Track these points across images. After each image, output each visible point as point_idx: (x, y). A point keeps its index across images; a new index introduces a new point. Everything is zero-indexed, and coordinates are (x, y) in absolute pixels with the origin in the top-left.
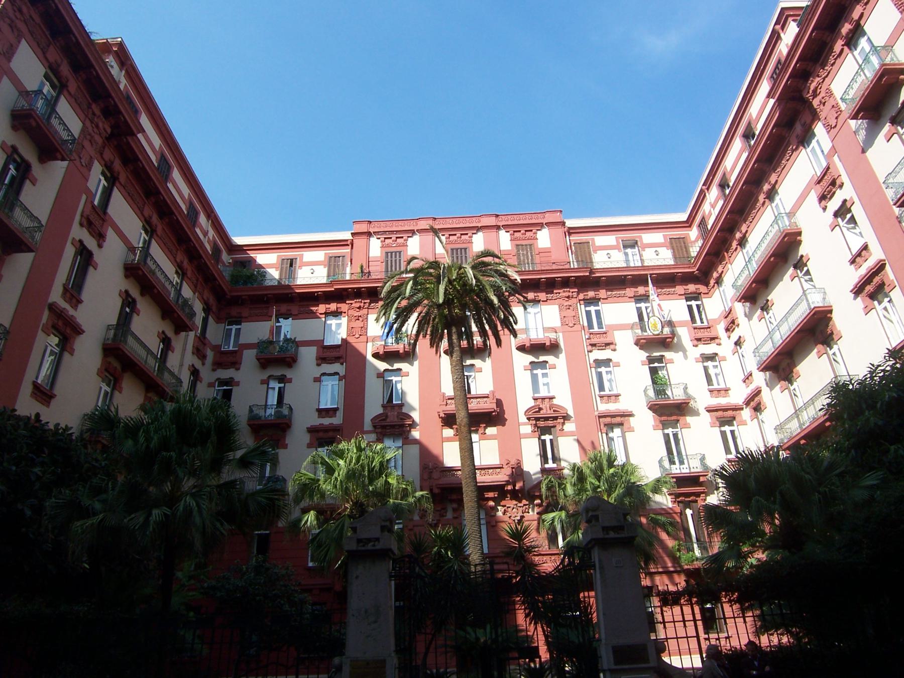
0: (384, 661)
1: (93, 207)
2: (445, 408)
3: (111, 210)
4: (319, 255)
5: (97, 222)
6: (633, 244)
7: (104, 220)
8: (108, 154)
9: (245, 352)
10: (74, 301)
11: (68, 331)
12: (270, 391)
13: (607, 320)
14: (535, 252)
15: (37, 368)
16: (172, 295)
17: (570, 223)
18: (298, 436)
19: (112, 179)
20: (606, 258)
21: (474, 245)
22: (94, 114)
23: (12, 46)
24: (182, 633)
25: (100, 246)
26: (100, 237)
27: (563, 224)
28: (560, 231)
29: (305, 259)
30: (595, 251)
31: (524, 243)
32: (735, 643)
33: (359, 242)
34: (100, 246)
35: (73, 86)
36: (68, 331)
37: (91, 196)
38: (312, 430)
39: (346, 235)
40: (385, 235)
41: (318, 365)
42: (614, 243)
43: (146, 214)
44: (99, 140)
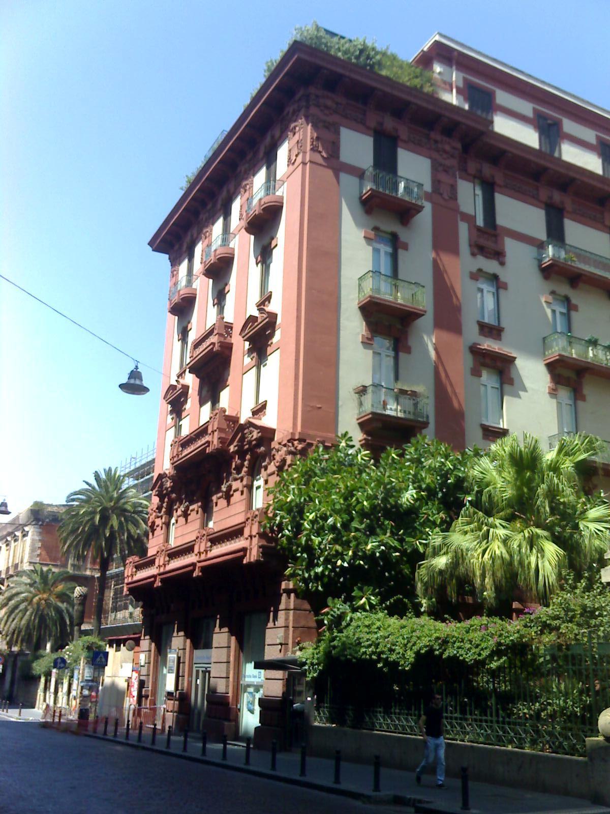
1: (479, 229)
3: (501, 221)
5: (489, 244)
7: (496, 236)
8: (472, 166)
10: (495, 332)
11: (499, 364)
12: (477, 197)
15: (273, 678)
16: (111, 572)
19: (489, 189)
20: (17, 715)
22: (436, 142)
23: (334, 143)
25: (502, 264)
26: (498, 255)
34: (502, 264)
35: (403, 132)
36: (499, 364)
37: (470, 219)
43: (372, 124)
44: (453, 162)
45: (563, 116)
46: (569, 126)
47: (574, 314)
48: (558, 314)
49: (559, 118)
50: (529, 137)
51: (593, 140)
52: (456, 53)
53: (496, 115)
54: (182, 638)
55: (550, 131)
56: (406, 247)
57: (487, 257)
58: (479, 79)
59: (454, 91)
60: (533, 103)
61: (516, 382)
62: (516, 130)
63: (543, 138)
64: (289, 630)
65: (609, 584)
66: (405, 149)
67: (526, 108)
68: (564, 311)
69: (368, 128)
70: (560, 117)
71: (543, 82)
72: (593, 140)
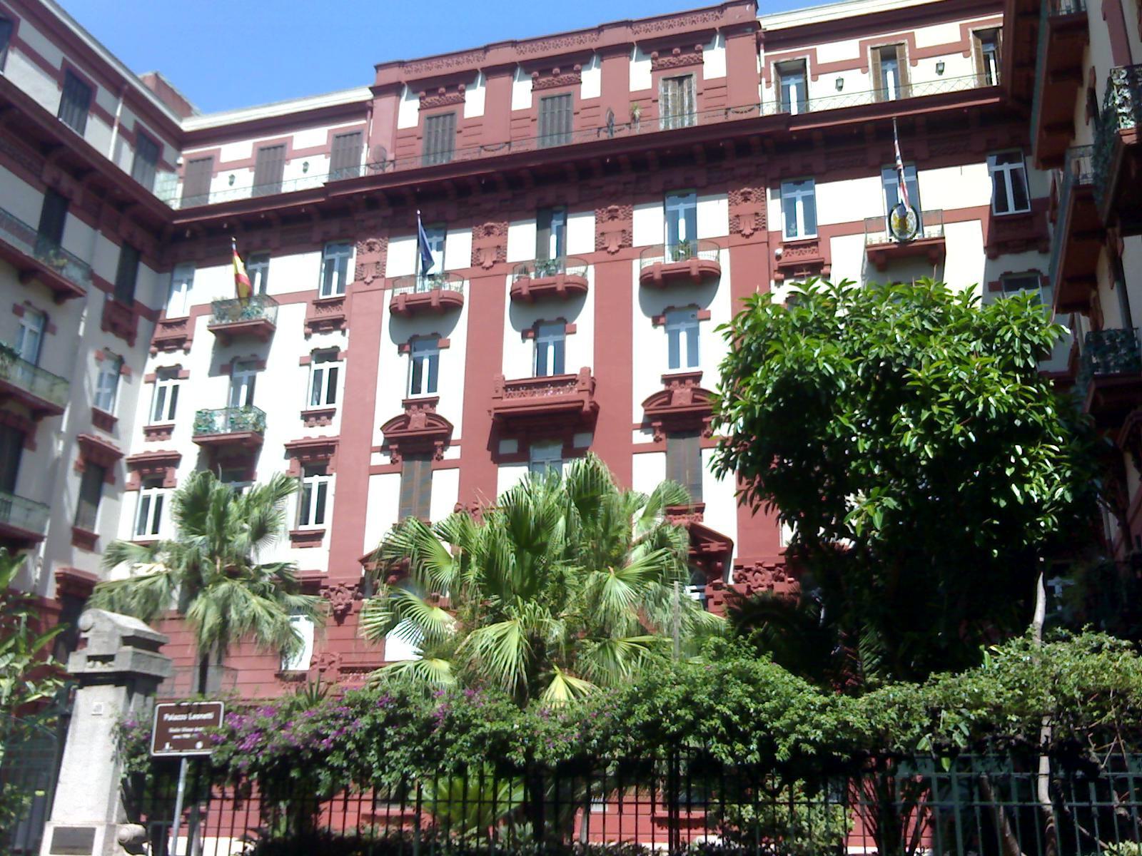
0: (94, 830)
2: (498, 403)
4: (318, 136)
6: (799, 70)
7: (131, 313)
9: (834, 241)
13: (928, 203)
14: (576, 107)
17: (770, 23)
18: (271, 464)
21: (583, 86)
24: (149, 776)
27: (756, 25)
28: (748, 41)
29: (821, 60)
30: (914, 62)
31: (556, 92)
32: (336, 826)
33: (383, 104)
38: (294, 451)
39: (364, 94)
40: (657, 48)
41: (307, 336)
42: (956, 37)
43: (47, 178)
45: (101, 83)
46: (103, 96)
47: (49, 337)
48: (106, 377)
49: (160, 142)
50: (45, 94)
51: (57, 64)
52: (126, 87)
53: (12, 50)
54: (206, 839)
55: (78, 94)
56: (53, 332)
57: (117, 335)
58: (89, 80)
59: (116, 128)
60: (65, 52)
61: (117, 482)
62: (103, 139)
63: (66, 101)
64: (950, 789)
65: (3, 677)
66: (77, 215)
67: (55, 56)
68: (37, 329)
69: (41, 182)
70: (18, 14)
71: (64, 13)
72: (57, 64)
